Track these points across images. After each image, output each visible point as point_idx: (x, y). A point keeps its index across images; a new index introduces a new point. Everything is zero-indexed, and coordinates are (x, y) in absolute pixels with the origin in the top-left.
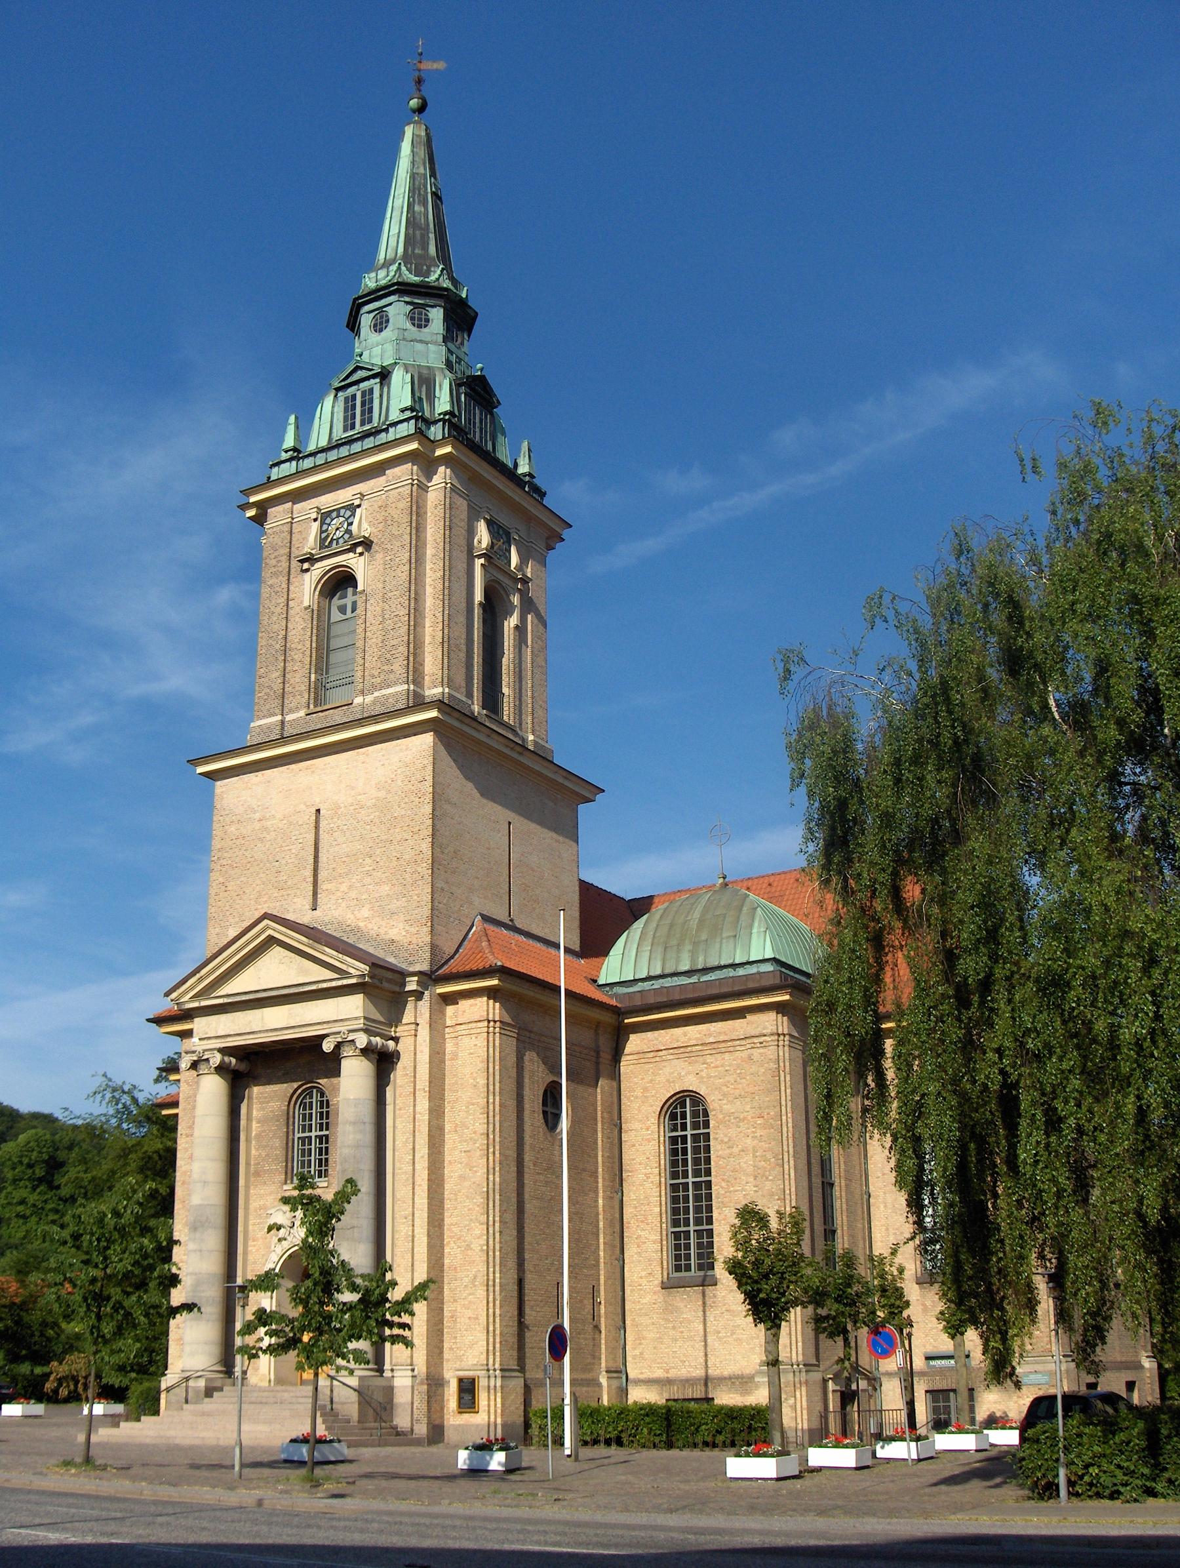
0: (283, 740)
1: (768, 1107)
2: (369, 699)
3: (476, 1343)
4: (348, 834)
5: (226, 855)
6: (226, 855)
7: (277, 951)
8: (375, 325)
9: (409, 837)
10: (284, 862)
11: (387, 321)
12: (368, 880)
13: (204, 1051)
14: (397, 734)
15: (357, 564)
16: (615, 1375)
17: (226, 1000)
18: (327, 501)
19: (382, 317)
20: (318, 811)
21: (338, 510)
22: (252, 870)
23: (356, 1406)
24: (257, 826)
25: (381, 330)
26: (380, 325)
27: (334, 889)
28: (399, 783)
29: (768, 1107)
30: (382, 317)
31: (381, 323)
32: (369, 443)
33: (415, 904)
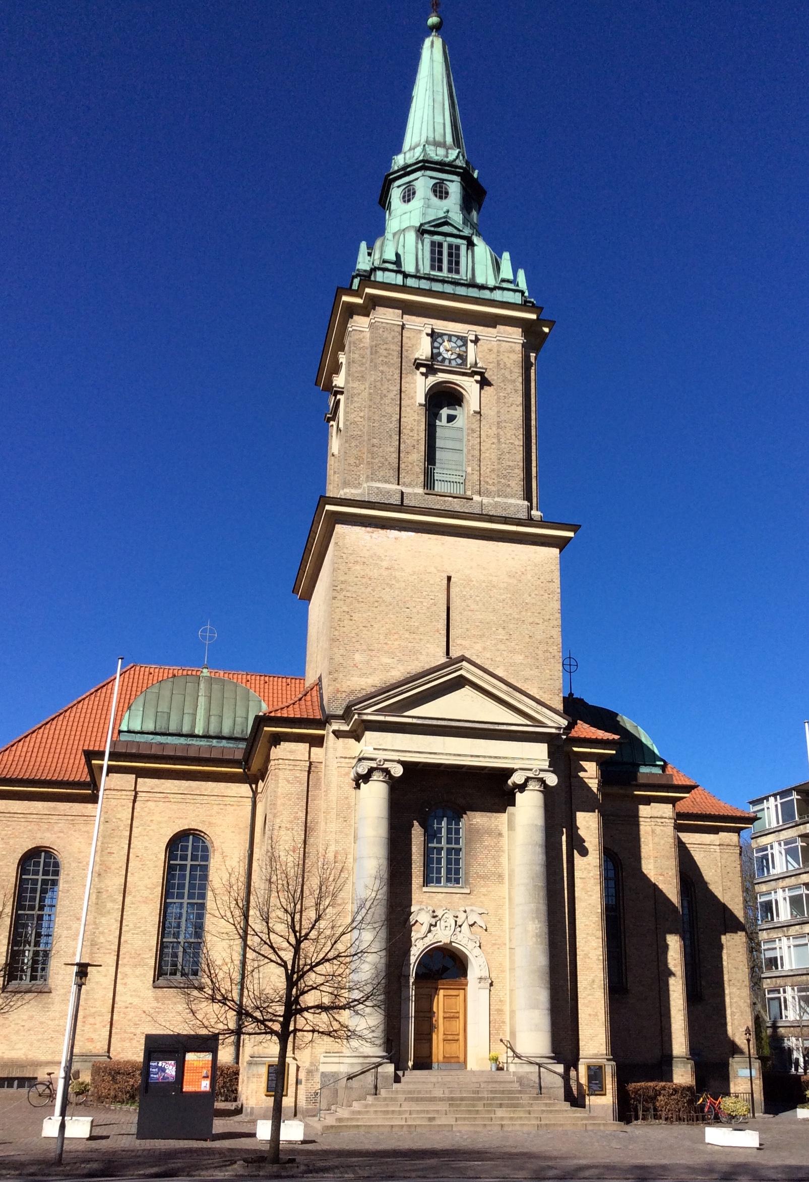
0: (401, 507)
1: (667, 869)
2: (486, 500)
3: (596, 1036)
4: (480, 604)
5: (350, 588)
6: (350, 588)
7: (467, 691)
8: (404, 197)
9: (540, 621)
10: (415, 610)
11: (414, 193)
12: (502, 647)
13: (386, 760)
14: (543, 540)
15: (469, 386)
16: (450, 1037)
17: (415, 721)
18: (441, 326)
19: (409, 191)
20: (449, 578)
21: (450, 336)
22: (380, 609)
23: (563, 1090)
24: (385, 573)
25: (409, 201)
26: (408, 196)
27: (468, 646)
28: (529, 577)
29: (667, 869)
30: (409, 191)
31: (409, 195)
32: (449, 289)
33: (548, 676)
